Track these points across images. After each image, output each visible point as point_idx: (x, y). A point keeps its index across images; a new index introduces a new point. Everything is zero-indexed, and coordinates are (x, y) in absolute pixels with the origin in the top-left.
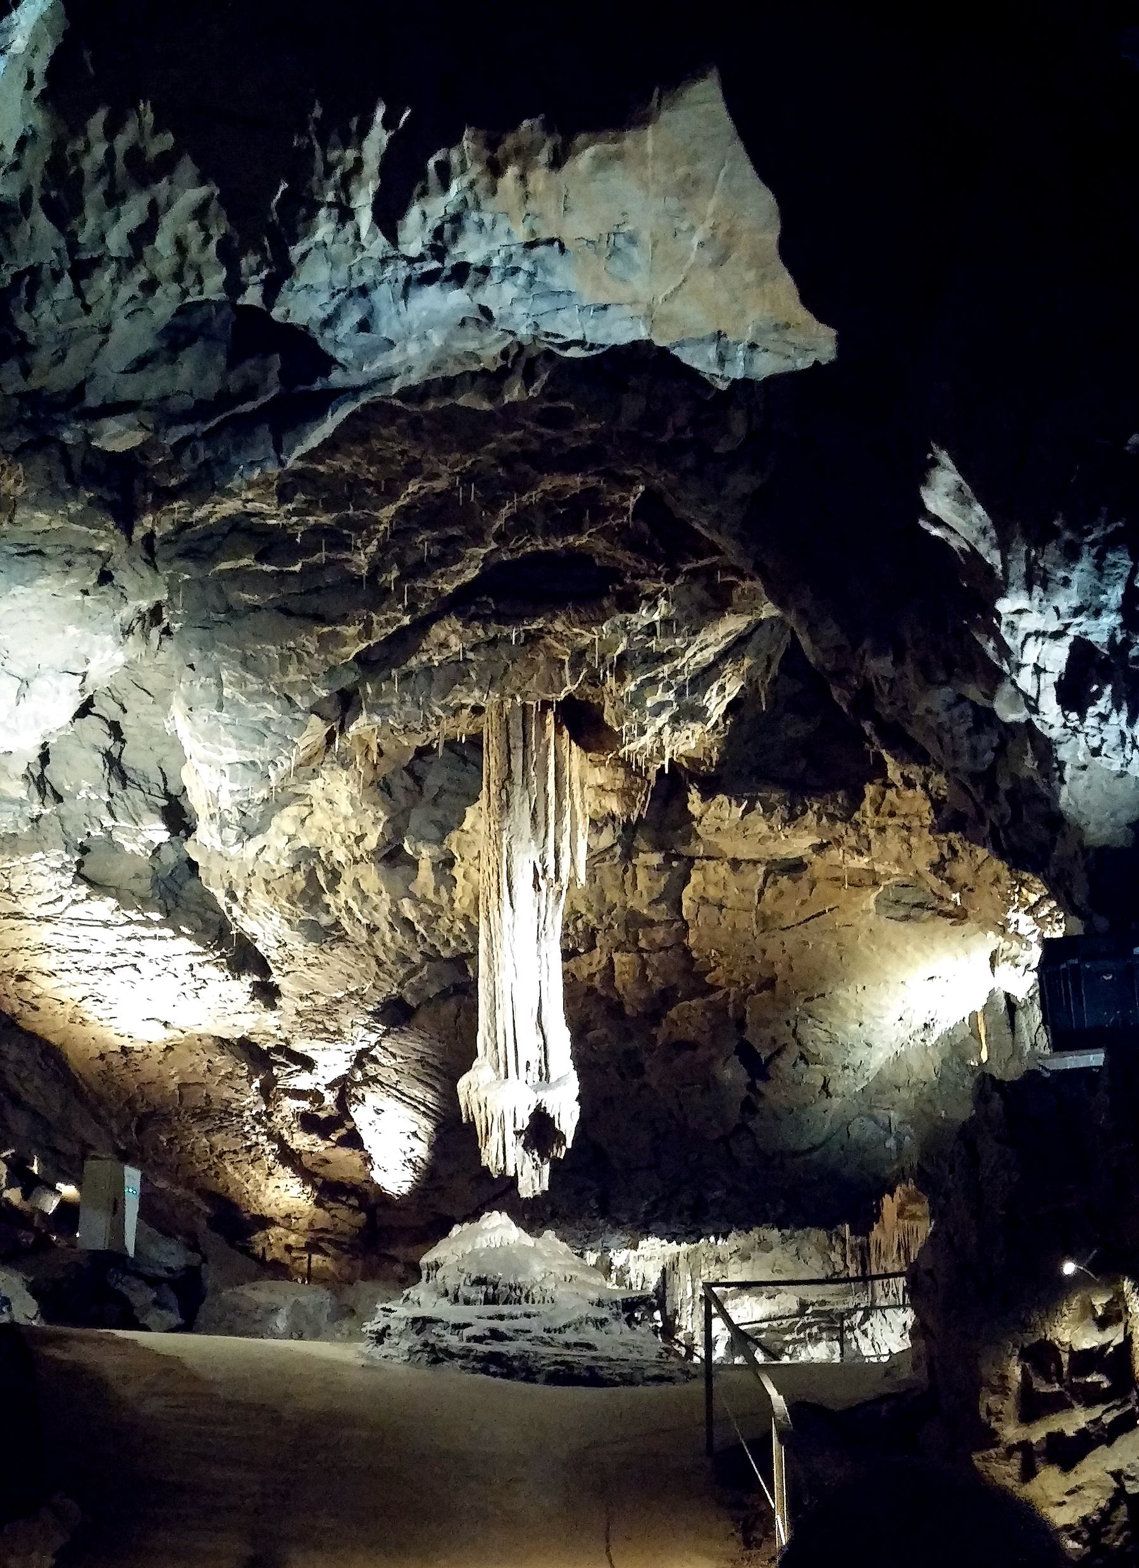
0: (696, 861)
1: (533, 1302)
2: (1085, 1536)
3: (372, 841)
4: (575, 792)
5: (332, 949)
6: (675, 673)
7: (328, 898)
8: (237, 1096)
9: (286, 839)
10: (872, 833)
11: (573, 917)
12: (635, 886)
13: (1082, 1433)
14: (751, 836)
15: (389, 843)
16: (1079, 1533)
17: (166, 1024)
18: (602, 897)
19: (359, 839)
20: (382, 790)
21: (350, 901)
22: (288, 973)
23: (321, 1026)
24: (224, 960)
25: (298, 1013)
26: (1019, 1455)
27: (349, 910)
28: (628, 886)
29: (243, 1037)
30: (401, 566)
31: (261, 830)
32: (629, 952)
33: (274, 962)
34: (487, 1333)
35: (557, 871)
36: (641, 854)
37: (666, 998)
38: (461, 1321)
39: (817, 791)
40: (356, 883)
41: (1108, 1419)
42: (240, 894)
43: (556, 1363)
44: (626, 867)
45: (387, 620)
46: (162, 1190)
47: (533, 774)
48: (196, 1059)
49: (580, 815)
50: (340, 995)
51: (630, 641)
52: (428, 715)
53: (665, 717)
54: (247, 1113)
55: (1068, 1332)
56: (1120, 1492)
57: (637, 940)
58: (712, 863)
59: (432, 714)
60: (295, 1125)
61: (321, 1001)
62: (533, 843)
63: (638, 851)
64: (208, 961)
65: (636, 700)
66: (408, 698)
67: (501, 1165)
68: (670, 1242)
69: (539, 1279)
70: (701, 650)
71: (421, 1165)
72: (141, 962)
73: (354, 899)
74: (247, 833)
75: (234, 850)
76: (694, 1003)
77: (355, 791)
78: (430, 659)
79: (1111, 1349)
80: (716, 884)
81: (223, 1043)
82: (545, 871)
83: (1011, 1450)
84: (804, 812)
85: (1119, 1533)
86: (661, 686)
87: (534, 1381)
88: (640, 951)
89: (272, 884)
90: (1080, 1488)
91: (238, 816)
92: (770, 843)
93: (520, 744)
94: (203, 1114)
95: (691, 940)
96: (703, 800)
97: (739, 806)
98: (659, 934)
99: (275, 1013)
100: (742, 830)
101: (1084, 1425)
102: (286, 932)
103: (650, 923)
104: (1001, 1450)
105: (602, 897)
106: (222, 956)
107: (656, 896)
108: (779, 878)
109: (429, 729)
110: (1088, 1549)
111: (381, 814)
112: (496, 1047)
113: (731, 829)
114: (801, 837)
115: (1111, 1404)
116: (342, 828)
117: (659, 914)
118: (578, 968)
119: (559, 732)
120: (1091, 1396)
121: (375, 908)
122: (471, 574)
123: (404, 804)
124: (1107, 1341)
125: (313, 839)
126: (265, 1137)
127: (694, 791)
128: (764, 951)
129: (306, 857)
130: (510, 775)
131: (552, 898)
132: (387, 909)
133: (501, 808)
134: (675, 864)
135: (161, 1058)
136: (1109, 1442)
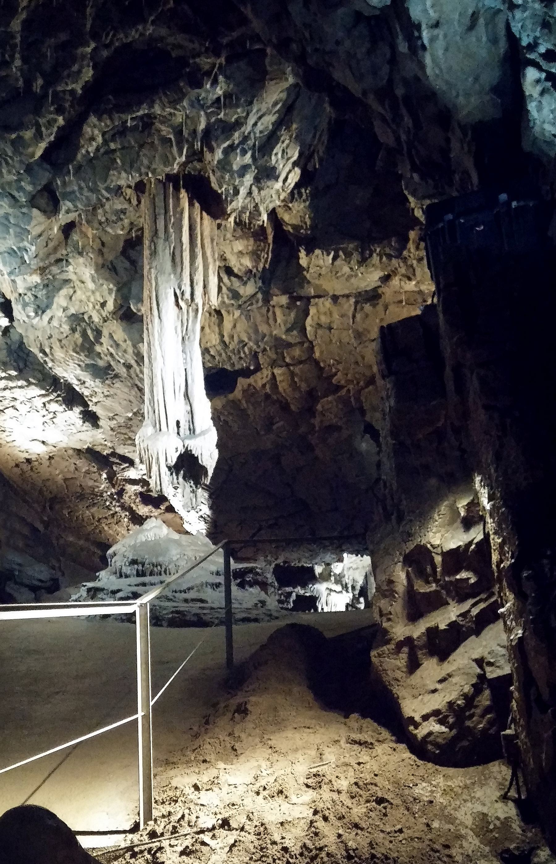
0: (312, 300)
1: (170, 574)
2: (451, 720)
3: (110, 306)
4: (206, 245)
5: (113, 384)
6: (245, 139)
7: (98, 348)
8: (96, 484)
9: (62, 310)
10: (415, 262)
11: (241, 345)
12: (275, 321)
13: (453, 625)
14: (340, 277)
15: (122, 306)
16: (446, 717)
17: (43, 442)
18: (256, 331)
19: (103, 305)
20: (110, 270)
21: (109, 348)
22: (96, 403)
23: (127, 437)
24: (60, 399)
25: (112, 429)
26: (405, 649)
27: (111, 355)
28: (271, 321)
29: (88, 448)
30: (43, 76)
31: (48, 306)
32: (282, 367)
33: (87, 396)
34: (130, 595)
35: (192, 294)
36: (274, 297)
37: (312, 396)
38: (115, 588)
39: (379, 241)
40: (111, 336)
41: (475, 611)
42: (47, 350)
43: (172, 612)
44: (268, 308)
45: (48, 122)
46: (71, 542)
47: (171, 230)
48: (67, 463)
49: (210, 260)
50: (130, 415)
51: (208, 115)
52: (100, 197)
53: (249, 179)
54: (105, 495)
55: (439, 535)
56: (482, 677)
57: (284, 358)
58: (322, 300)
59: (103, 196)
60: (137, 500)
61: (121, 420)
62: (172, 276)
63: (272, 296)
64: (51, 400)
65: (224, 165)
66: (83, 184)
67: (158, 488)
68: (357, 555)
69: (175, 559)
70: (260, 118)
71: (209, 519)
72: (17, 404)
73: (111, 346)
74: (40, 310)
75: (36, 321)
76: (330, 398)
77: (93, 272)
78: (87, 152)
79: (473, 546)
80: (325, 314)
81: (79, 452)
82: (183, 294)
83: (400, 645)
84: (371, 255)
85: (483, 716)
86: (238, 151)
87: (161, 626)
88: (288, 365)
89: (63, 342)
90: (450, 676)
91: (33, 299)
92: (353, 280)
93: (163, 211)
94: (81, 497)
95: (317, 355)
96: (307, 255)
97: (328, 254)
98: (297, 352)
99: (100, 431)
100: (334, 272)
101: (454, 619)
102: (78, 372)
103: (289, 345)
104: (392, 646)
105: (256, 331)
106: (59, 396)
107: (289, 325)
108: (364, 305)
109: (121, 220)
110: (454, 732)
111: (111, 286)
112: (154, 412)
113: (327, 273)
114: (371, 272)
115: (478, 598)
116: (92, 299)
117: (293, 337)
118: (256, 381)
119: (191, 204)
120: (462, 593)
121: (125, 351)
122: (88, 74)
123: (125, 279)
124: (470, 540)
125: (77, 307)
126: (120, 508)
127: (302, 251)
128: (363, 358)
129: (77, 320)
130: (156, 232)
131: (191, 314)
132: (132, 351)
133: (151, 255)
134: (298, 303)
135: (48, 464)
136: (477, 632)
